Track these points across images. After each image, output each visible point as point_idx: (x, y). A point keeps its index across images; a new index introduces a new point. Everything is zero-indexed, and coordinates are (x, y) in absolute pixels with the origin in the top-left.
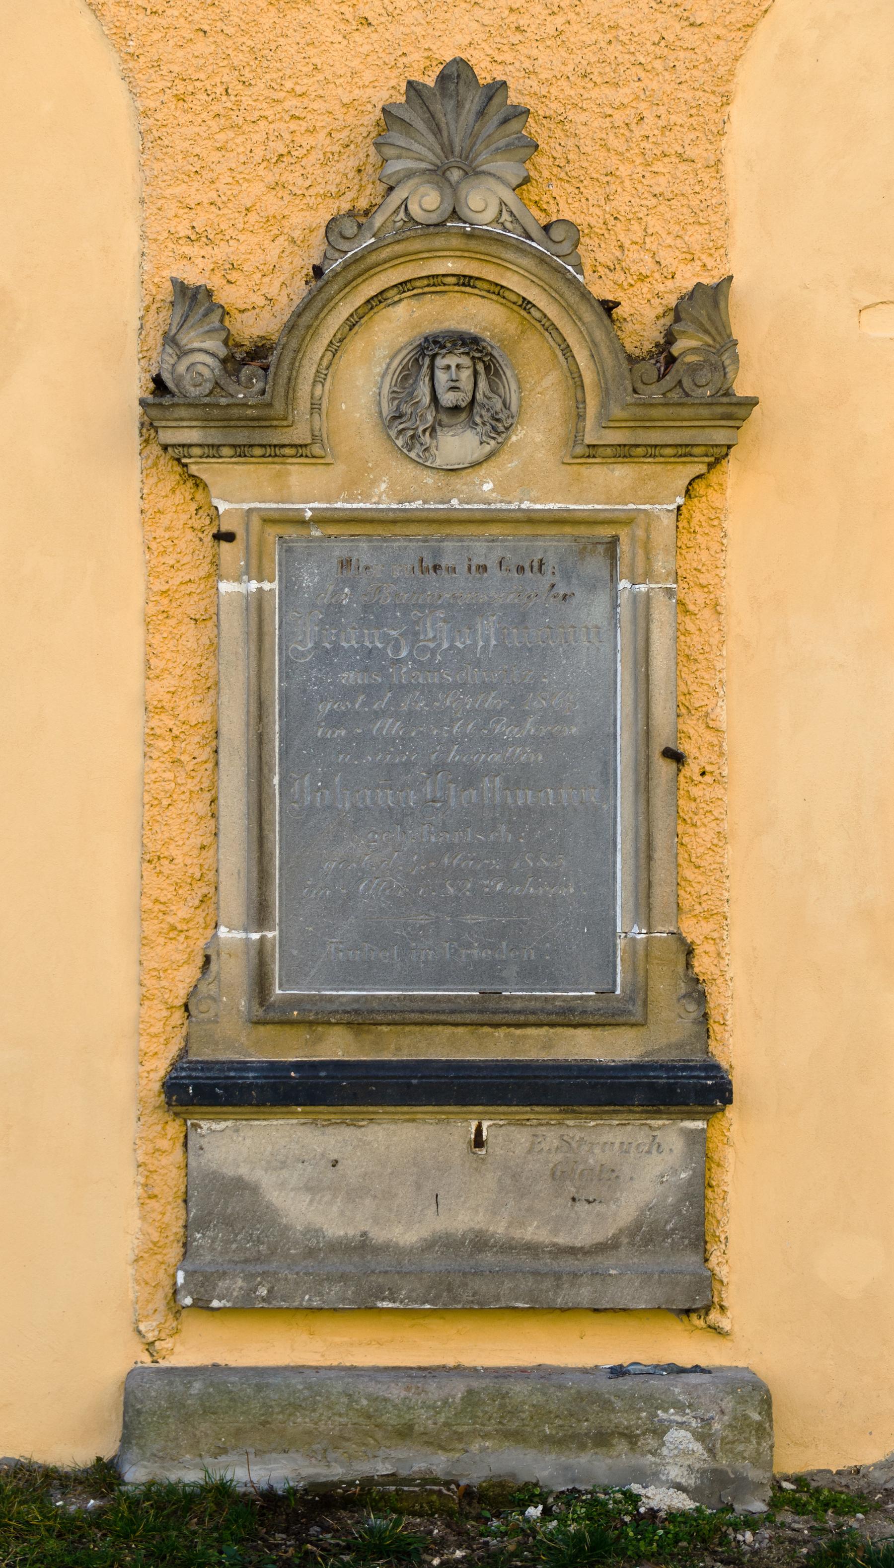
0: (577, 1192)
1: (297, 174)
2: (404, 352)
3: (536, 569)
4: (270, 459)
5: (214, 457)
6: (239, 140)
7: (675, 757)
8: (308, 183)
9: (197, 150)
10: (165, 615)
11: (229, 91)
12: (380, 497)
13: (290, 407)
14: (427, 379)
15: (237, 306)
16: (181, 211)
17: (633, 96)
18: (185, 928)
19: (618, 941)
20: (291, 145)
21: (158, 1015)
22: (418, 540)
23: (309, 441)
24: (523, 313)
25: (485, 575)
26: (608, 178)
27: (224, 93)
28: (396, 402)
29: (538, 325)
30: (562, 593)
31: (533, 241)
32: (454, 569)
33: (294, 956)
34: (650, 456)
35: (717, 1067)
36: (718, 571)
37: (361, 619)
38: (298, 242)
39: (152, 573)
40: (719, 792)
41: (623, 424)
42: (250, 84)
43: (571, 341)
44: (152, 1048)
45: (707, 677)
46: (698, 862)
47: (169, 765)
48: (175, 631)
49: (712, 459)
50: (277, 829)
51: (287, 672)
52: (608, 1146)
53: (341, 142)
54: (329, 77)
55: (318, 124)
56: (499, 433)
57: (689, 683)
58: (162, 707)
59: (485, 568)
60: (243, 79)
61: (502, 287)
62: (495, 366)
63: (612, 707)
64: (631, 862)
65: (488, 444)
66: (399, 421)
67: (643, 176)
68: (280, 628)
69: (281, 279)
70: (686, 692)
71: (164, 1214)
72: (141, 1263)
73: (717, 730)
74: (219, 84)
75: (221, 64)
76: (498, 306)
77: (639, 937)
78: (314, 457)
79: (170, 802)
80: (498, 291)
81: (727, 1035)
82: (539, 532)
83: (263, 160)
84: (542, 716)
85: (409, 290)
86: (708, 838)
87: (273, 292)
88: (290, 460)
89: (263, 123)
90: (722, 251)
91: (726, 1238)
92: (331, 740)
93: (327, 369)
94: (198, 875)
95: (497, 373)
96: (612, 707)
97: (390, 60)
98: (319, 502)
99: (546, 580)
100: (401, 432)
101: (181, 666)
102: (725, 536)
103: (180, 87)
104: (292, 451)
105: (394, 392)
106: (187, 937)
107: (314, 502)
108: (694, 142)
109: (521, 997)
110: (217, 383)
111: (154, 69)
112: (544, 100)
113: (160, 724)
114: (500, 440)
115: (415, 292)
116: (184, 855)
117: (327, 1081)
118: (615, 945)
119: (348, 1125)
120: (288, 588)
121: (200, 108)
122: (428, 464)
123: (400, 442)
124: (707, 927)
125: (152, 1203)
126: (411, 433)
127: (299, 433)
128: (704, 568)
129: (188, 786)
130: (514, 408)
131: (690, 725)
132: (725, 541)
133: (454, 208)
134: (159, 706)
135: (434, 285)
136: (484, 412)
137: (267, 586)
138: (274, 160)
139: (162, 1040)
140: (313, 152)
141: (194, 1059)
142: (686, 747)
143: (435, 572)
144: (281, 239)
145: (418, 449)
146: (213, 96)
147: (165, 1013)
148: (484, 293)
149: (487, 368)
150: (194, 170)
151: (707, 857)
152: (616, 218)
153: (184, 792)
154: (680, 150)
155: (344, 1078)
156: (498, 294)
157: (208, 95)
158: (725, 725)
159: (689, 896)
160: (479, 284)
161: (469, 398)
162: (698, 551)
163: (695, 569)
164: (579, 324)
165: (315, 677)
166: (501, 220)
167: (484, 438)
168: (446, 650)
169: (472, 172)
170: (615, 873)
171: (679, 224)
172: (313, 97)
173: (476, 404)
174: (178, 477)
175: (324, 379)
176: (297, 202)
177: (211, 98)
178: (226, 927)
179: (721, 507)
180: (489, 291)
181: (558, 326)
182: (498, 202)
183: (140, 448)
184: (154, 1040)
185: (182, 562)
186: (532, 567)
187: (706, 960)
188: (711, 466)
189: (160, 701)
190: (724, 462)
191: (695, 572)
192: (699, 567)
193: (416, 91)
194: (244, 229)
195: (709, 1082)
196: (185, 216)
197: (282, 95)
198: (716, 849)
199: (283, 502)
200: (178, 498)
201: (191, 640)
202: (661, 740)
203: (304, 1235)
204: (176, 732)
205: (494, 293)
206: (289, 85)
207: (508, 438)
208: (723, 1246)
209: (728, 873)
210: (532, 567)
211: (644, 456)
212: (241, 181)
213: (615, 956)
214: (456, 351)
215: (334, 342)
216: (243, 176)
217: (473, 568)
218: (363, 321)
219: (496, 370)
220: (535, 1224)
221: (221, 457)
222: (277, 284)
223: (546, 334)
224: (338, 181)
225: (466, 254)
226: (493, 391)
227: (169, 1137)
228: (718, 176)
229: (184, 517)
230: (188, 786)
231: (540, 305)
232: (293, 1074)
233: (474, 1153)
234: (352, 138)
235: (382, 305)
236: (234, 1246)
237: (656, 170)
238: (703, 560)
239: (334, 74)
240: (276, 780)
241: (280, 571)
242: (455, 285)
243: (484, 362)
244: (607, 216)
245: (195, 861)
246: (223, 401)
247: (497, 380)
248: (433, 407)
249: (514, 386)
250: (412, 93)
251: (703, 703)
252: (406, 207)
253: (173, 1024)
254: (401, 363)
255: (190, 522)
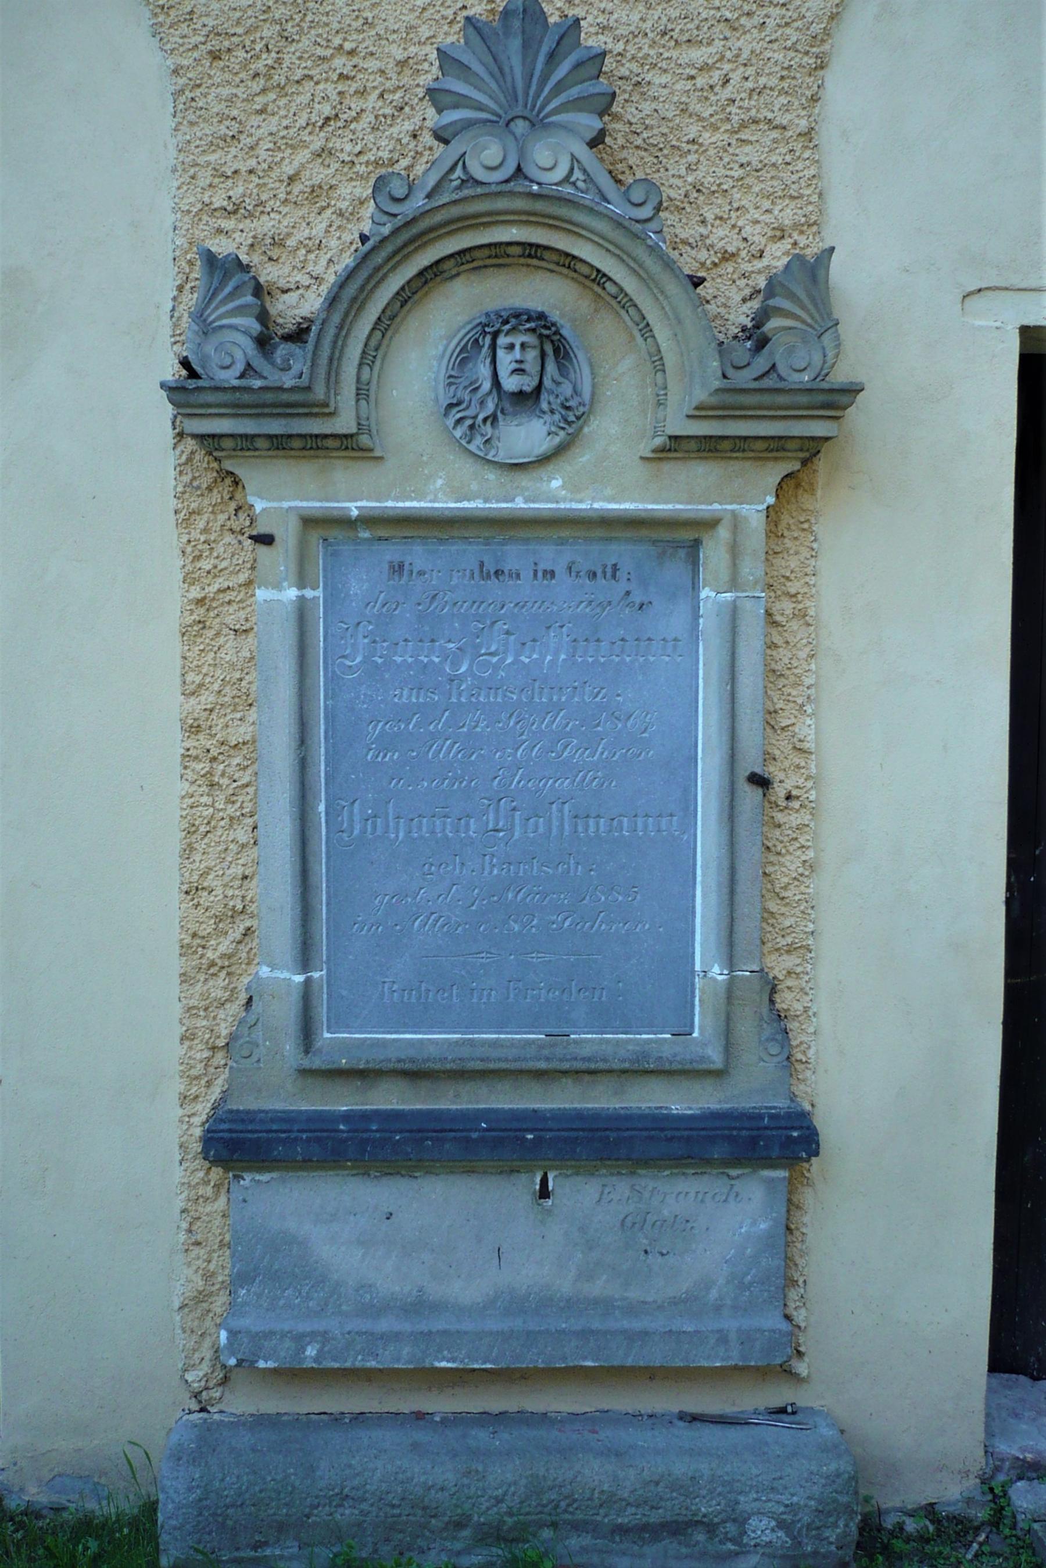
0: (650, 1244)
1: (345, 139)
2: (463, 332)
3: (609, 575)
4: (312, 452)
5: (249, 449)
6: (282, 102)
7: (760, 782)
8: (358, 148)
9: (235, 113)
10: (201, 626)
11: (270, 47)
12: (436, 496)
13: (332, 391)
14: (488, 360)
15: (280, 285)
16: (216, 180)
17: (718, 56)
18: (227, 963)
19: (697, 980)
20: (339, 107)
21: (198, 1056)
22: (478, 543)
23: (354, 430)
24: (596, 288)
25: (553, 581)
26: (690, 147)
27: (265, 50)
28: (453, 388)
29: (613, 303)
30: (638, 601)
31: (609, 203)
32: (518, 576)
33: (343, 997)
34: (738, 451)
35: (804, 1115)
36: (807, 579)
37: (415, 630)
38: (347, 214)
39: (189, 579)
40: (805, 817)
41: (710, 413)
42: (293, 40)
43: (650, 318)
44: (193, 1091)
45: (794, 693)
46: (784, 894)
47: (205, 788)
48: (213, 643)
49: (806, 455)
50: (324, 861)
51: (333, 689)
52: (682, 1196)
53: (394, 104)
54: (382, 32)
55: (369, 85)
56: (570, 423)
57: (775, 700)
58: (199, 726)
59: (552, 574)
60: (286, 34)
61: (574, 257)
62: (564, 347)
63: (693, 727)
64: (713, 898)
65: (557, 434)
66: (458, 409)
67: (729, 144)
68: (325, 640)
69: (328, 256)
70: (772, 709)
71: (209, 1262)
72: (186, 1310)
73: (805, 752)
74: (258, 40)
75: (262, 17)
76: (569, 281)
77: (720, 978)
78: (362, 449)
79: (208, 829)
80: (568, 262)
81: (808, 1073)
82: (613, 535)
83: (308, 124)
84: (615, 738)
85: (468, 262)
86: (793, 867)
87: (319, 269)
88: (335, 454)
89: (308, 85)
90: (815, 228)
91: (805, 1281)
92: (382, 763)
93: (376, 350)
94: (239, 907)
95: (567, 354)
96: (693, 727)
97: (449, 13)
98: (368, 500)
99: (622, 586)
100: (459, 421)
101: (219, 681)
102: (815, 540)
103: (215, 43)
104: (336, 443)
105: (451, 376)
106: (228, 974)
107: (361, 500)
108: (786, 108)
109: (590, 1040)
110: (248, 365)
111: (187, 23)
112: (619, 58)
113: (196, 744)
114: (570, 431)
115: (475, 264)
116: (225, 886)
117: (378, 1135)
118: (693, 985)
119: (403, 1176)
120: (333, 597)
121: (237, 67)
122: (489, 457)
123: (458, 433)
124: (790, 961)
125: (196, 1251)
126: (469, 422)
127: (344, 423)
128: (793, 575)
129: (228, 812)
130: (586, 396)
131: (781, 746)
132: (815, 545)
133: (519, 165)
134: (195, 725)
135: (496, 256)
136: (552, 398)
137: (309, 593)
138: (319, 124)
139: (203, 1082)
140: (364, 115)
141: (235, 1108)
142: (773, 771)
143: (498, 578)
144: (329, 211)
145: (479, 440)
146: (253, 53)
147: (206, 1054)
148: (552, 266)
149: (557, 351)
150: (231, 134)
151: (791, 887)
152: (698, 191)
153: (223, 819)
154: (770, 116)
155: (396, 1132)
156: (569, 267)
157: (247, 52)
158: (813, 745)
159: (771, 929)
160: (547, 255)
161: (535, 383)
162: (786, 557)
163: (783, 576)
164: (661, 298)
165: (365, 694)
166: (573, 179)
167: (553, 429)
168: (509, 664)
169: (538, 123)
170: (694, 907)
171: (768, 198)
172: (362, 54)
173: (543, 390)
174: (215, 474)
175: (373, 362)
176: (346, 170)
177: (249, 55)
178: (268, 966)
179: (811, 508)
180: (558, 264)
181: (638, 302)
182: (569, 158)
183: (173, 441)
184: (194, 1082)
185: (219, 568)
186: (604, 573)
187: (788, 996)
188: (805, 462)
189: (195, 719)
190: (815, 460)
191: (783, 580)
192: (788, 574)
193: (475, 28)
194: (286, 200)
195: (795, 1134)
196: (221, 186)
197: (328, 52)
198: (801, 879)
199: (328, 501)
200: (215, 497)
201: (230, 653)
202: (750, 763)
203: (357, 1291)
204: (214, 752)
205: (564, 265)
206: (337, 41)
207: (581, 428)
208: (802, 1291)
209: (814, 903)
210: (604, 573)
211: (731, 451)
212: (283, 147)
213: (693, 997)
214: (521, 327)
215: (383, 319)
216: (285, 141)
217: (540, 574)
218: (416, 297)
219: (567, 353)
220: (605, 1277)
221: (256, 449)
222: (323, 262)
223: (623, 312)
224: (390, 147)
225: (532, 219)
226: (562, 375)
227: (212, 1184)
228: (811, 145)
229: (222, 518)
230: (228, 812)
231: (616, 277)
232: (342, 1127)
233: (539, 1205)
234: (406, 99)
235: (438, 279)
236: (282, 1302)
237: (743, 137)
238: (793, 566)
239: (386, 28)
240: (322, 808)
241: (325, 577)
242: (520, 256)
243: (552, 342)
244: (689, 188)
245: (237, 892)
246: (258, 383)
247: (567, 364)
248: (495, 392)
249: (586, 370)
250: (471, 29)
251: (789, 722)
252: (464, 163)
253: (215, 1064)
254: (458, 344)
255: (229, 523)
